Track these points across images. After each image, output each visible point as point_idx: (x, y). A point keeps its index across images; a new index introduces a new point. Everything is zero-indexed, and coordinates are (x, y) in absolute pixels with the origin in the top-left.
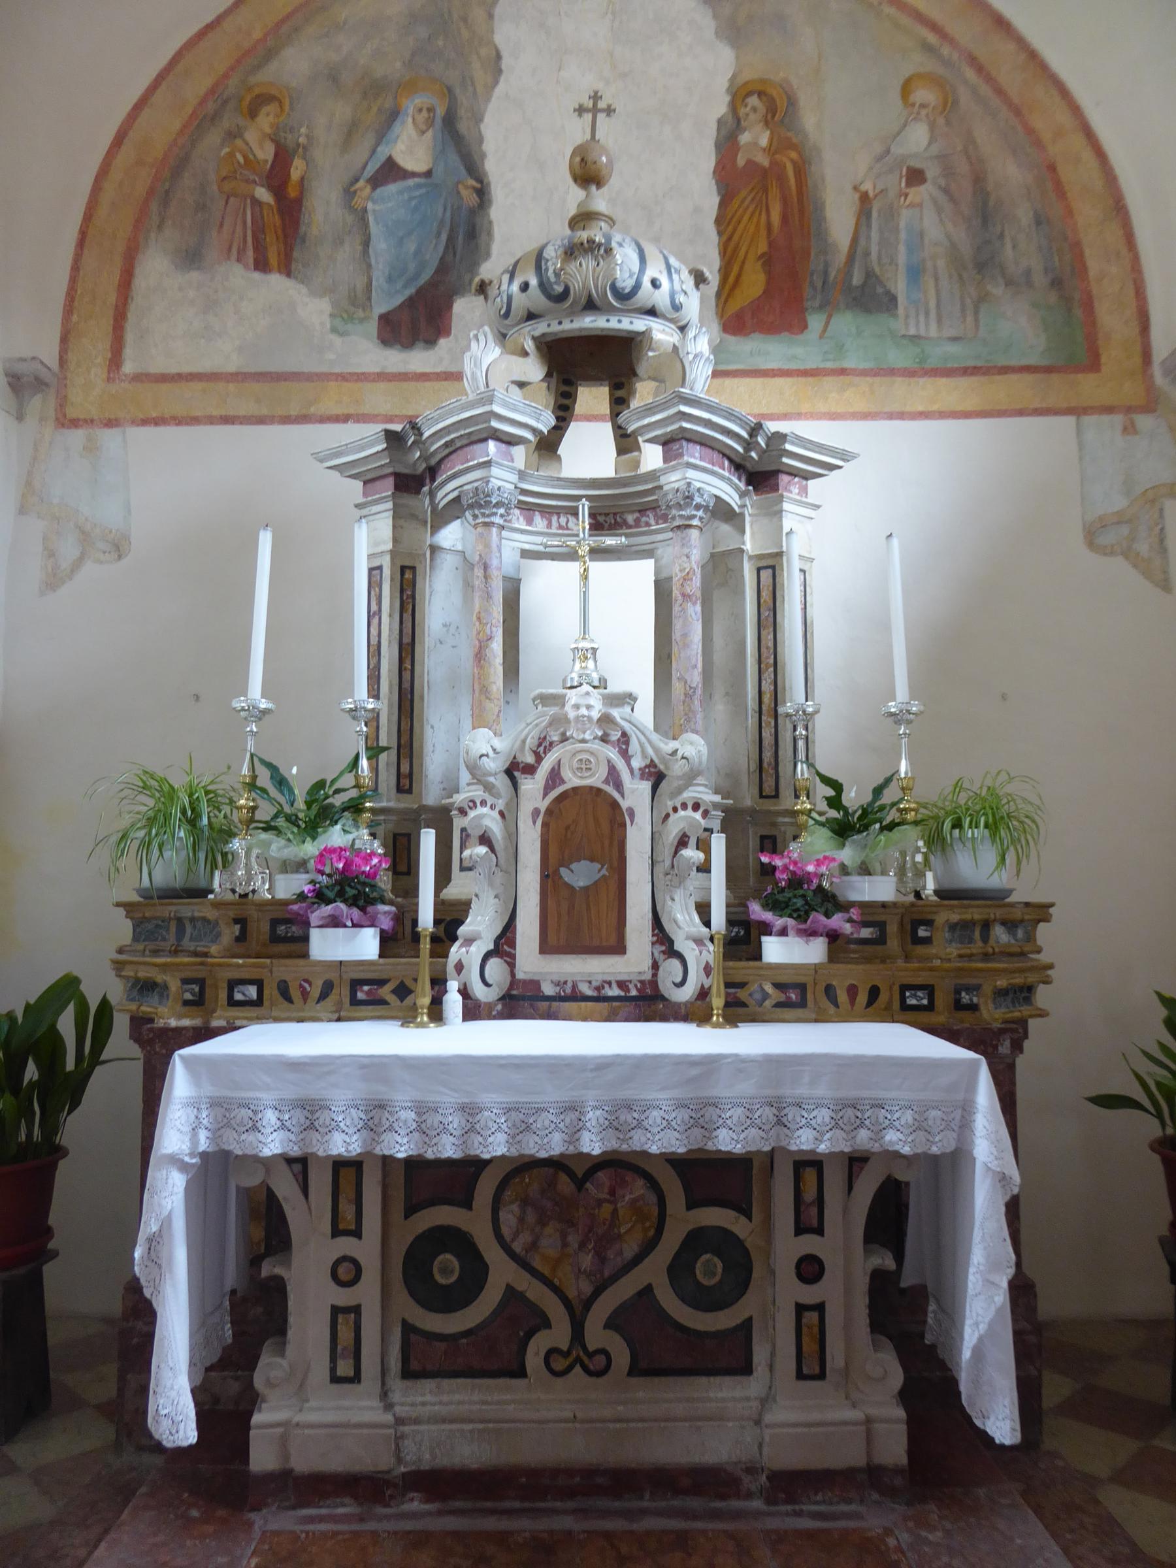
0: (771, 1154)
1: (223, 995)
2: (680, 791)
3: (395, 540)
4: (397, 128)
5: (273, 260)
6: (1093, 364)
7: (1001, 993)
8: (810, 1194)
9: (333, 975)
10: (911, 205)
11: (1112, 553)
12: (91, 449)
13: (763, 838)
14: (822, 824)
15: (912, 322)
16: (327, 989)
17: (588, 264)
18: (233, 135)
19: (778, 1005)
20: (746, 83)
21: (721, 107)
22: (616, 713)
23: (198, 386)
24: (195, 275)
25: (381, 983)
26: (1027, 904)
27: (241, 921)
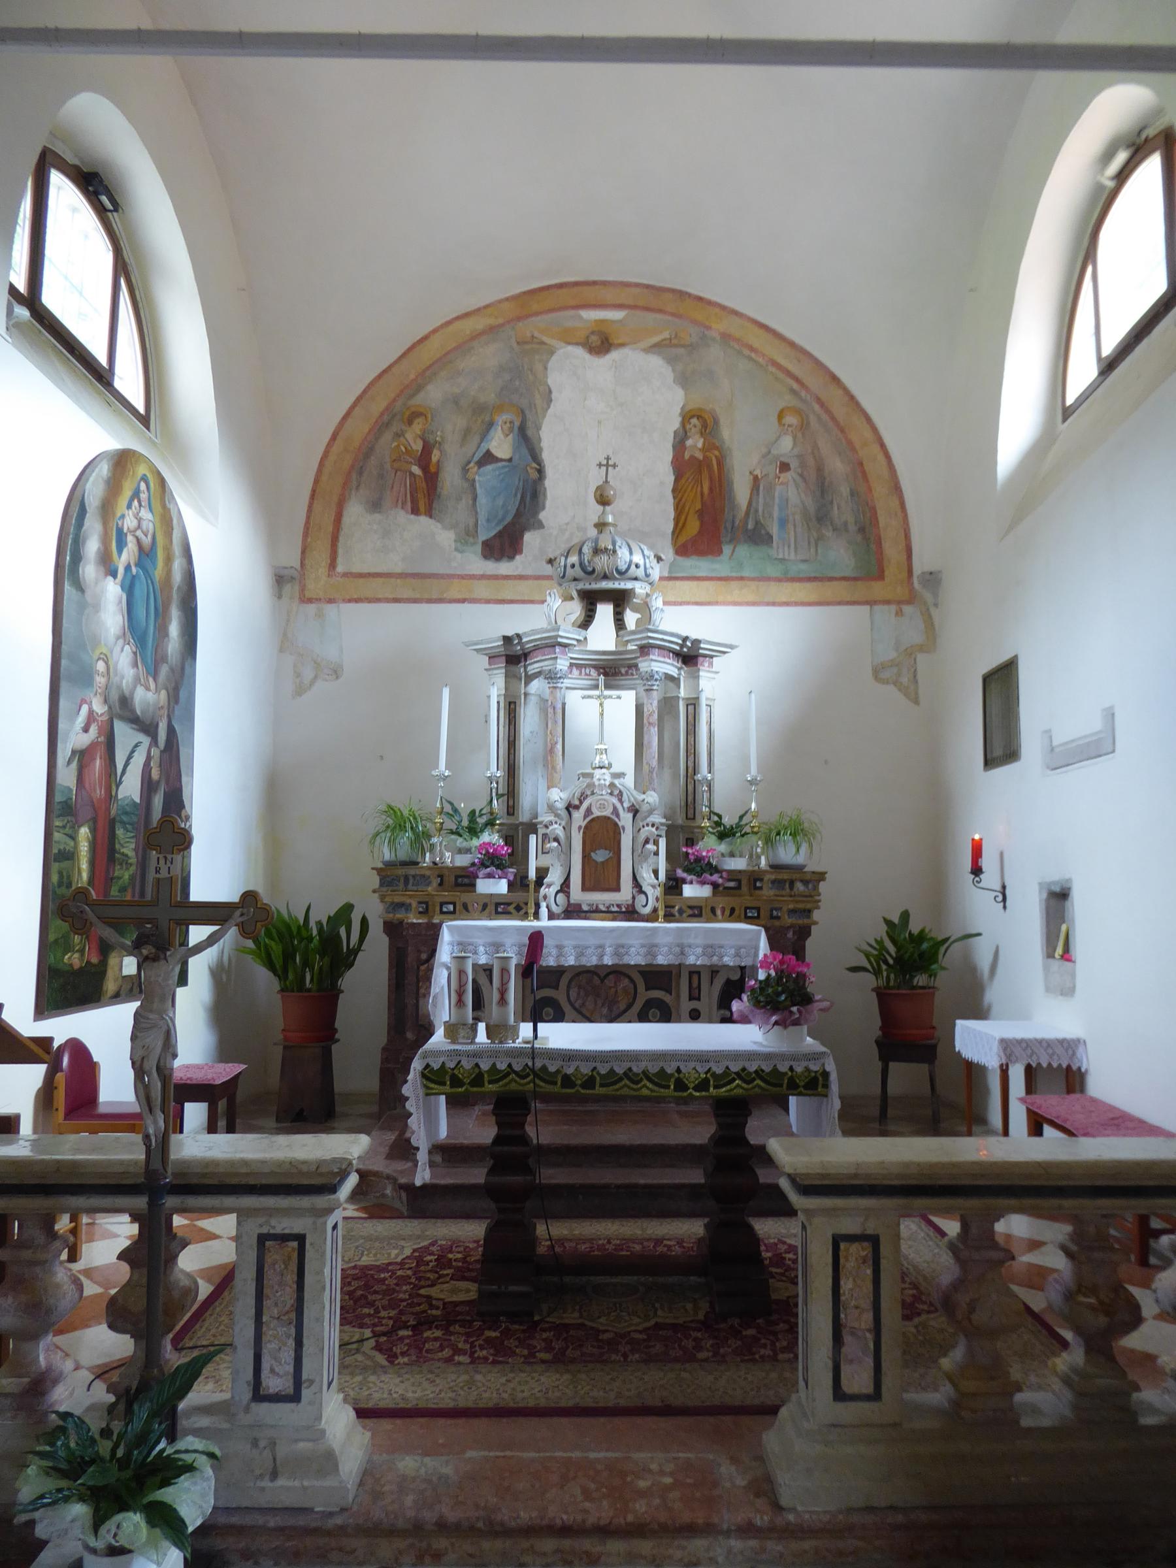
0: (680, 964)
1: (438, 909)
2: (646, 818)
3: (506, 689)
4: (492, 432)
5: (422, 508)
6: (881, 576)
7: (792, 912)
8: (695, 984)
9: (486, 900)
10: (782, 484)
11: (888, 683)
12: (320, 615)
13: (687, 839)
14: (714, 833)
15: (780, 550)
16: (485, 907)
17: (604, 558)
18: (399, 435)
19: (690, 916)
20: (690, 411)
21: (676, 424)
22: (616, 782)
23: (380, 580)
24: (377, 516)
25: (509, 904)
26: (813, 872)
27: (441, 876)
